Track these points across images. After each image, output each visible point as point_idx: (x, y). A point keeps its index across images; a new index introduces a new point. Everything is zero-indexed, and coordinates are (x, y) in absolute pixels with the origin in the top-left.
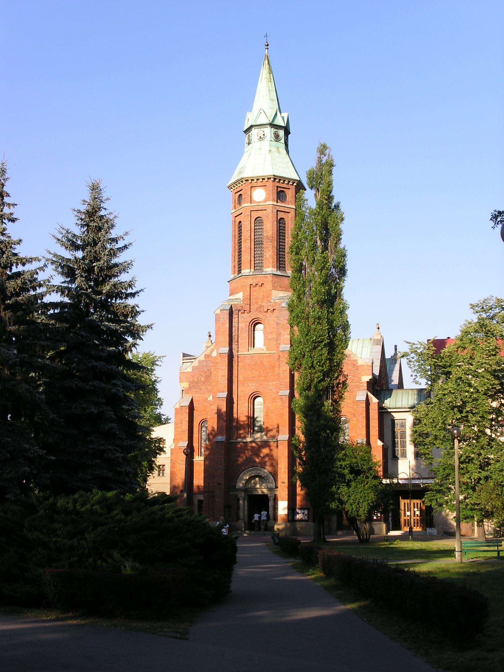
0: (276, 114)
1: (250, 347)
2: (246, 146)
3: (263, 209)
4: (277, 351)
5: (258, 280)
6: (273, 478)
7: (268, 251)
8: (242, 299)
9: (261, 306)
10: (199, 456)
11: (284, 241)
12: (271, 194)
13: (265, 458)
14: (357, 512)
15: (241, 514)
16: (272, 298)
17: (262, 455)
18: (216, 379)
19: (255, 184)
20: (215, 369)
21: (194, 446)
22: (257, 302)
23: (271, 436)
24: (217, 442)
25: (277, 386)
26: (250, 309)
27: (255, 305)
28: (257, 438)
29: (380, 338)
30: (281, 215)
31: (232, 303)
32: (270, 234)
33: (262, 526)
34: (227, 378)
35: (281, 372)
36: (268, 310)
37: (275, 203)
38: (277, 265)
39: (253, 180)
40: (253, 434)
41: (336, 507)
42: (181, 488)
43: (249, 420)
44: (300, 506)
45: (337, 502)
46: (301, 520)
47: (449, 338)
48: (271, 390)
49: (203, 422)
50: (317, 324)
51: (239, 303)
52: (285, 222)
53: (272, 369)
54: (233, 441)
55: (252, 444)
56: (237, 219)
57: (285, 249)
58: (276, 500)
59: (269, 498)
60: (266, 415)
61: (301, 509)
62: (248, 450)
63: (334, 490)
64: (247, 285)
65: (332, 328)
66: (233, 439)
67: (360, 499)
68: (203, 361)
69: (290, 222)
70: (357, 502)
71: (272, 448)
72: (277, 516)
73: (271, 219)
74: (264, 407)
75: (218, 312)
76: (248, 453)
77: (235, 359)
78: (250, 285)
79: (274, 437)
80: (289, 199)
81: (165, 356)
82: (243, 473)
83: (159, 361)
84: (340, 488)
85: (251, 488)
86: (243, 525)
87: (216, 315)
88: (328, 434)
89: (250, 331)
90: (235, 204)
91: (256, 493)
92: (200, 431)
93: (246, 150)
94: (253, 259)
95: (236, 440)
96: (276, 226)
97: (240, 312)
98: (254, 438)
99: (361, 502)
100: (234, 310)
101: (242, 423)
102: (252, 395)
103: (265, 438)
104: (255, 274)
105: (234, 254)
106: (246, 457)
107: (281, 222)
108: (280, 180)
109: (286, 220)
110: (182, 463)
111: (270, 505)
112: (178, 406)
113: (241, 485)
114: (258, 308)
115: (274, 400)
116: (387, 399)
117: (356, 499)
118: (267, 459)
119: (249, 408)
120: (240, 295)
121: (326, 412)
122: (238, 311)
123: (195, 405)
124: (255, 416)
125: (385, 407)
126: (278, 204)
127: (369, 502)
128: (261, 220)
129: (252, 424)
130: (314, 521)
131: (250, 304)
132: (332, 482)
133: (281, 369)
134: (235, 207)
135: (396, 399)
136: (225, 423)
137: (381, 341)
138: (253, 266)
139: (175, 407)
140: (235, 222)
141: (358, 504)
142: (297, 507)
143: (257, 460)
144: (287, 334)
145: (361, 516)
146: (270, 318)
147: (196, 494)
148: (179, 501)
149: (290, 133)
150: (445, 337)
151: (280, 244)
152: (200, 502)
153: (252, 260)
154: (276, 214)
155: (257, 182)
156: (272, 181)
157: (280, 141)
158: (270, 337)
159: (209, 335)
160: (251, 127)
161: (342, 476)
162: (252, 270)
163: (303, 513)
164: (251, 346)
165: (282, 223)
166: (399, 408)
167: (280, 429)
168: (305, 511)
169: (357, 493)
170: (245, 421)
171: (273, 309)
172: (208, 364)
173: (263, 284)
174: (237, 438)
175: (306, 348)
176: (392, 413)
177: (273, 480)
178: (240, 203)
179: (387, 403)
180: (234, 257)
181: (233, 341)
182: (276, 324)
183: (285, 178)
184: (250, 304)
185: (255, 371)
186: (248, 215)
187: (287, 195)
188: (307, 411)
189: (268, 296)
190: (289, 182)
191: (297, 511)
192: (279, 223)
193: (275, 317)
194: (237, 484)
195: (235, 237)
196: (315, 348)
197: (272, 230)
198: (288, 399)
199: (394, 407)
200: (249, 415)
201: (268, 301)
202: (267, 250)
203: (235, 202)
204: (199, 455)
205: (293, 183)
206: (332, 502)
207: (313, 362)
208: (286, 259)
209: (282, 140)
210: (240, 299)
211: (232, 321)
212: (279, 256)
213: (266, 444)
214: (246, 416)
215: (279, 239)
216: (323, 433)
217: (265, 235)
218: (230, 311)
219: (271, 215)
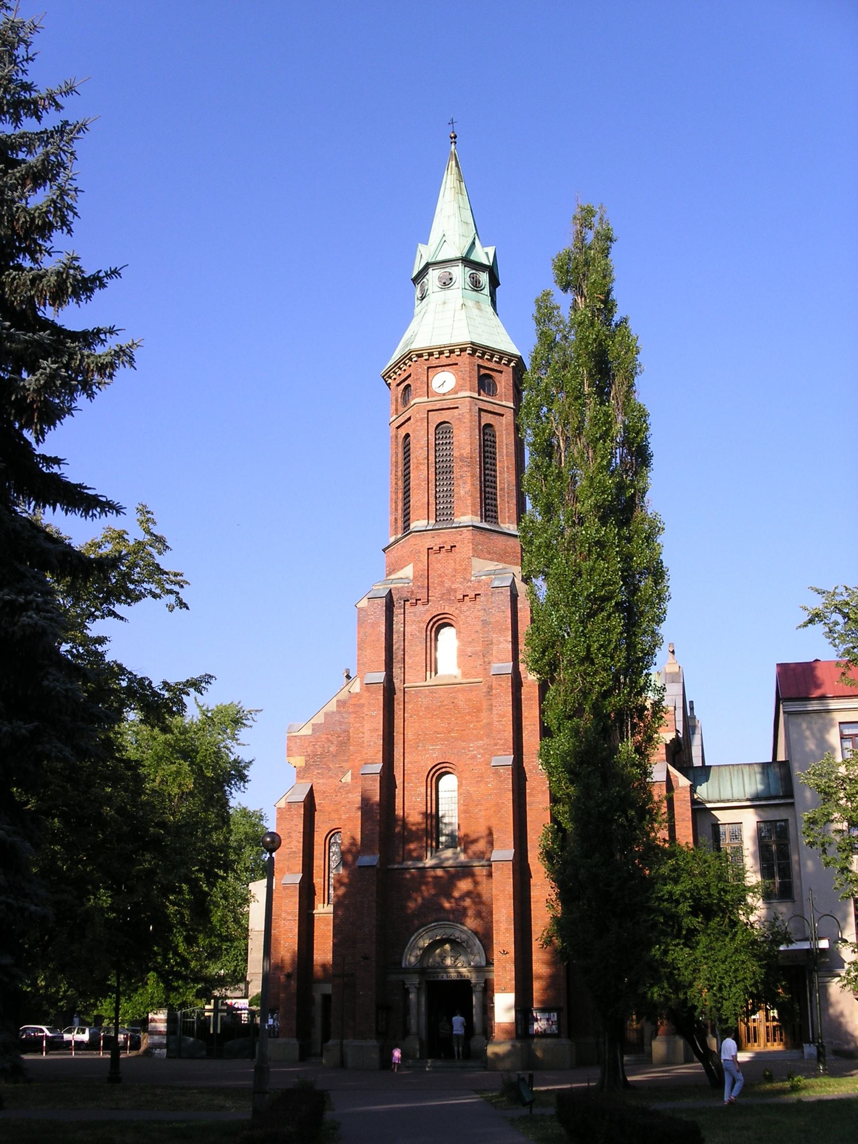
0: (473, 243)
1: (428, 673)
2: (416, 305)
3: (451, 406)
4: (484, 678)
5: (445, 538)
6: (480, 945)
7: (464, 483)
8: (411, 578)
9: (450, 591)
10: (325, 905)
11: (493, 467)
12: (468, 379)
13: (464, 901)
14: (719, 1010)
15: (413, 1022)
16: (473, 573)
17: (456, 894)
18: (359, 738)
19: (433, 361)
20: (356, 718)
21: (316, 885)
22: (443, 582)
23: (474, 853)
24: (360, 867)
25: (487, 749)
26: (428, 596)
27: (438, 588)
28: (447, 859)
29: (677, 670)
30: (487, 419)
31: (392, 586)
32: (466, 451)
33: (456, 1048)
34: (382, 733)
35: (495, 719)
36: (464, 596)
37: (476, 395)
38: (481, 511)
39: (431, 354)
40: (436, 851)
41: (662, 1000)
42: (288, 969)
43: (429, 822)
44: (542, 1002)
45: (666, 986)
46: (543, 1035)
47: (817, 660)
48: (474, 757)
49: (333, 832)
50: (597, 559)
51: (406, 585)
52: (495, 431)
53: (474, 714)
54: (396, 866)
55: (434, 871)
56: (400, 432)
57: (495, 482)
58: (488, 991)
59: (471, 988)
60: (465, 809)
61: (542, 1010)
62: (427, 884)
63: (657, 957)
64: (422, 549)
65: (629, 577)
66: (394, 863)
67: (723, 978)
68: (333, 712)
69: (504, 432)
70: (717, 984)
71: (479, 879)
72: (492, 1027)
73: (468, 424)
74: (459, 794)
75: (364, 603)
76: (428, 890)
77: (399, 696)
78: (428, 549)
79: (481, 856)
80: (501, 390)
81: (261, 710)
82: (416, 934)
83: (248, 719)
84: (669, 950)
85: (433, 967)
86: (418, 1047)
87: (360, 610)
88: (630, 821)
89: (428, 640)
90: (397, 405)
91: (445, 978)
92: (327, 852)
93: (417, 310)
94: (432, 500)
95: (401, 863)
96: (478, 437)
97: (409, 603)
98: (440, 859)
99: (727, 985)
100: (395, 600)
101: (414, 828)
102: (434, 770)
103: (463, 857)
104: (437, 527)
105: (394, 497)
106: (423, 898)
107: (486, 431)
108: (484, 354)
109: (497, 428)
110: (290, 917)
111: (474, 1003)
112: (282, 804)
113: (413, 959)
114: (444, 594)
115: (480, 779)
116: (701, 785)
117: (715, 976)
118: (468, 902)
119: (429, 798)
120: (408, 572)
121: (625, 766)
122: (405, 601)
123: (317, 801)
124: (440, 814)
125: (699, 800)
126: (481, 397)
127: (748, 983)
128: (448, 427)
129: (434, 831)
130: (569, 1037)
131: (428, 587)
132: (651, 935)
133: (495, 712)
134: (397, 410)
135: (719, 784)
136: (378, 828)
137: (680, 676)
138: (432, 514)
139: (278, 805)
140: (397, 437)
141: (720, 989)
142: (535, 1006)
143: (447, 905)
144: (506, 641)
145: (727, 1020)
146: (469, 614)
147: (319, 981)
148: (283, 995)
149: (499, 284)
150: (810, 659)
151: (487, 472)
152: (327, 998)
153: (430, 502)
154: (477, 414)
155: (439, 358)
156: (469, 354)
157: (482, 292)
158: (469, 650)
159: (346, 675)
160: (428, 266)
161: (673, 919)
162: (432, 521)
163: (548, 1020)
164: (431, 671)
165: (490, 435)
166: (728, 801)
167: (495, 836)
168: (552, 1014)
169: (714, 962)
170: (419, 824)
171: (476, 595)
172: (344, 718)
173: (455, 546)
174: (404, 860)
175: (574, 613)
176: (713, 812)
177: (481, 948)
178: (405, 402)
179: (702, 791)
180: (396, 502)
181: (394, 660)
182: (480, 623)
183: (493, 351)
184: (428, 587)
185: (439, 721)
186: (422, 419)
187: (497, 384)
188: (581, 763)
189: (465, 569)
190: (501, 359)
191: (535, 1014)
192: (484, 434)
193: (479, 611)
194: (404, 958)
195: (396, 466)
196: (592, 615)
197: (471, 444)
198: (511, 772)
199: (717, 797)
200: (429, 811)
201: (464, 579)
202: (461, 482)
203: (397, 401)
204: (324, 903)
205: (510, 361)
206: (652, 986)
207: (589, 647)
208: (498, 502)
209: (485, 289)
210: (407, 578)
211: (393, 620)
212: (485, 496)
213: (465, 871)
214: (422, 814)
215: (485, 463)
216: (620, 817)
217: (456, 453)
218: (388, 601)
219: (468, 416)
